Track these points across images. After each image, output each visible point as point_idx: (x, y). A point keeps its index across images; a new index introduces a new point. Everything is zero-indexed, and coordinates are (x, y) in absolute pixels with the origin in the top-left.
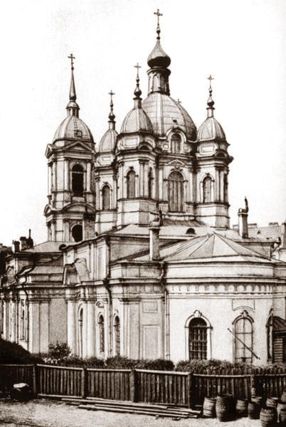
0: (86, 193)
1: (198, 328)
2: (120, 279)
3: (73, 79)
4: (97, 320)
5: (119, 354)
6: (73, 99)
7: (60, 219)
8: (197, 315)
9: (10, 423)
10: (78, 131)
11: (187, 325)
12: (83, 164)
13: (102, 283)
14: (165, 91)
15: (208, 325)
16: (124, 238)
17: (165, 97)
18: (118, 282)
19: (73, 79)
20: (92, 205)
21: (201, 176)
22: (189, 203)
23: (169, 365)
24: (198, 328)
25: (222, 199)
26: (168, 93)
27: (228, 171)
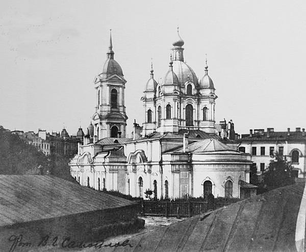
0: (120, 106)
1: (208, 185)
2: (171, 162)
3: (111, 40)
4: (164, 183)
5: (167, 196)
6: (111, 48)
7: (104, 122)
8: (208, 179)
9: (101, 232)
10: (114, 68)
11: (203, 184)
12: (117, 89)
13: (158, 163)
14: (182, 60)
15: (213, 184)
16: (168, 140)
17: (182, 62)
18: (170, 163)
19: (111, 40)
20: (122, 113)
21: (202, 106)
22: (195, 121)
23: (94, 189)
24: (208, 185)
25: (213, 119)
26: (183, 61)
27: (215, 104)
